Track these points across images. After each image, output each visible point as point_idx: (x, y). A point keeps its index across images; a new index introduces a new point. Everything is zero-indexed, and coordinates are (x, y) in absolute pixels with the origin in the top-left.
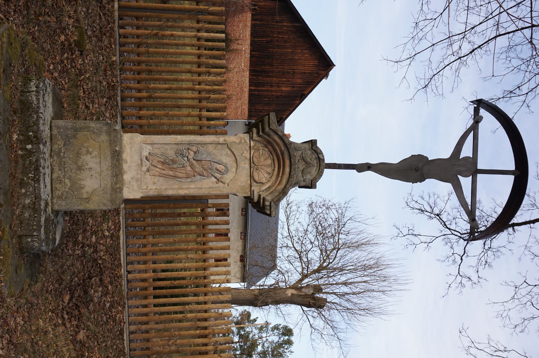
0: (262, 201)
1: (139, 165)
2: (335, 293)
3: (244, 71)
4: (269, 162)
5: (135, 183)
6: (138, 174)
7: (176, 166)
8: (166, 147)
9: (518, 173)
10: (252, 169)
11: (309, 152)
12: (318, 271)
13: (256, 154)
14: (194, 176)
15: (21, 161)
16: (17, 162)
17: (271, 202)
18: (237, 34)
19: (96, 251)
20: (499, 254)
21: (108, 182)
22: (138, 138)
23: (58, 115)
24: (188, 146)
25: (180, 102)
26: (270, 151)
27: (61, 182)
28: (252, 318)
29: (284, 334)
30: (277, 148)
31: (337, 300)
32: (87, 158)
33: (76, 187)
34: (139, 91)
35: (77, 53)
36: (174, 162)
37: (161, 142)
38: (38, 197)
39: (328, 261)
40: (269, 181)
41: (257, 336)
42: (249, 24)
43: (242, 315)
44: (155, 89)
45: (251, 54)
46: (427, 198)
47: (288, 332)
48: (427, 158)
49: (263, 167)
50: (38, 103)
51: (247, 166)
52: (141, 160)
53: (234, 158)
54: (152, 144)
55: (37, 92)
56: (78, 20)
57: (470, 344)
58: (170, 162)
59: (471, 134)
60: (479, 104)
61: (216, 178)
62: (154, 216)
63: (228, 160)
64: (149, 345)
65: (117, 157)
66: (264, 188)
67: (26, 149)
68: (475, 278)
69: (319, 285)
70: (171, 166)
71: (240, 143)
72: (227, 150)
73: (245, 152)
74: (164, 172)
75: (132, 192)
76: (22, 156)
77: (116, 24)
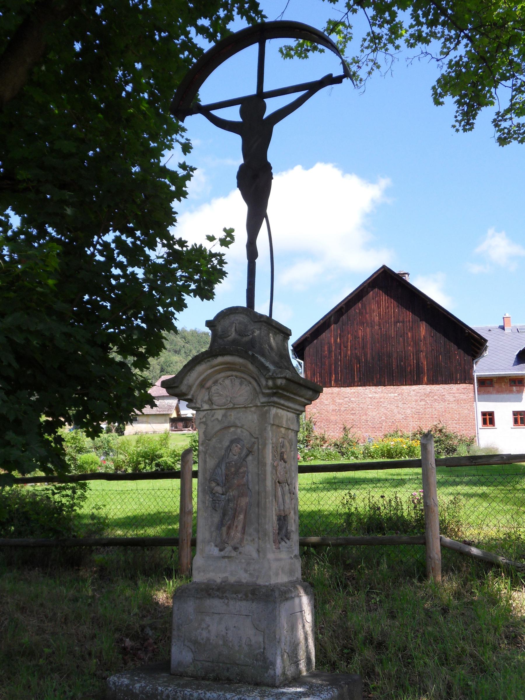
30: (205, 374)
48: (242, 167)
52: (224, 557)
59: (215, 113)
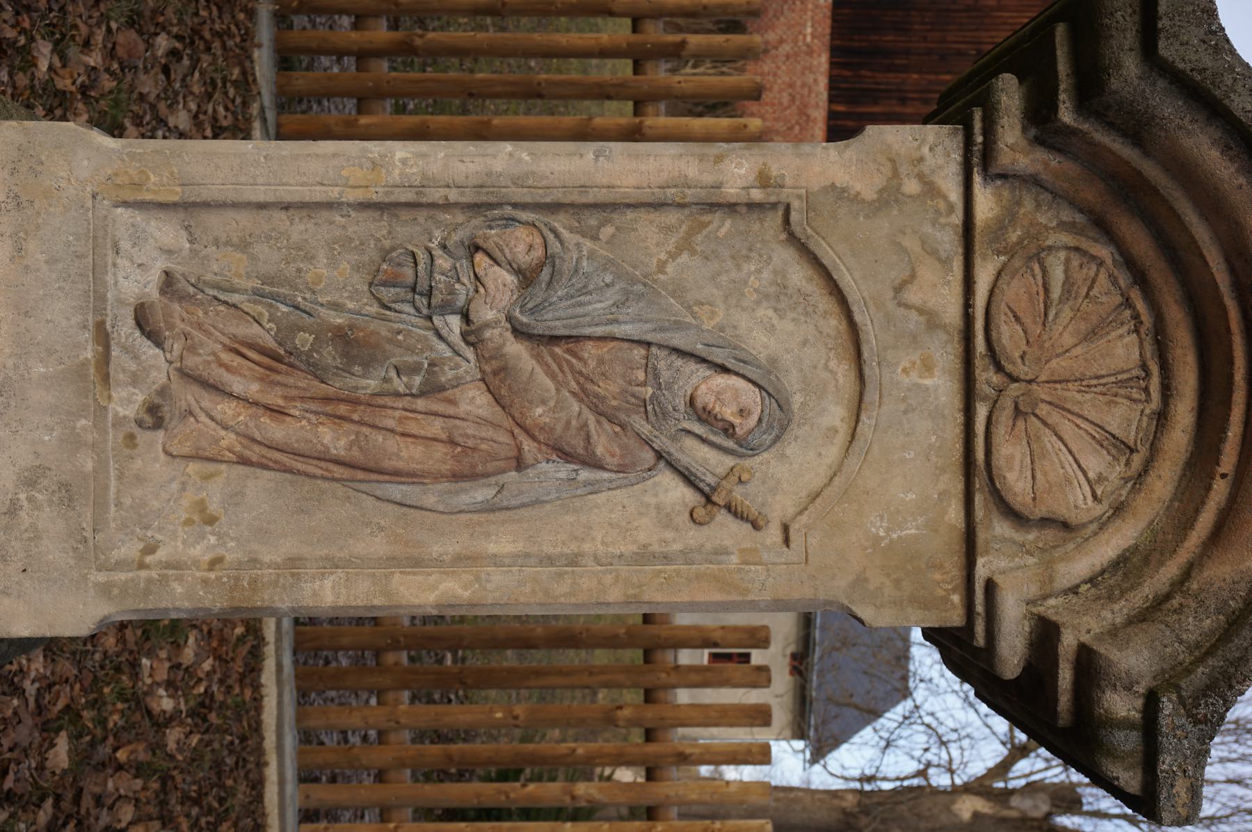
0: (1065, 676)
3: (810, 52)
4: (1123, 350)
6: (73, 442)
7: (372, 384)
8: (299, 229)
10: (982, 412)
13: (1016, 291)
14: (520, 464)
17: (1151, 701)
24: (466, 228)
25: (543, 73)
26: (1130, 263)
30: (1201, 232)
36: (353, 347)
37: (260, 195)
40: (1119, 509)
49: (1072, 394)
51: (943, 386)
52: (103, 336)
53: (834, 323)
54: (187, 208)
58: (329, 355)
61: (688, 478)
63: (786, 334)
70: (338, 385)
71: (889, 197)
72: (784, 256)
73: (928, 272)
74: (276, 431)
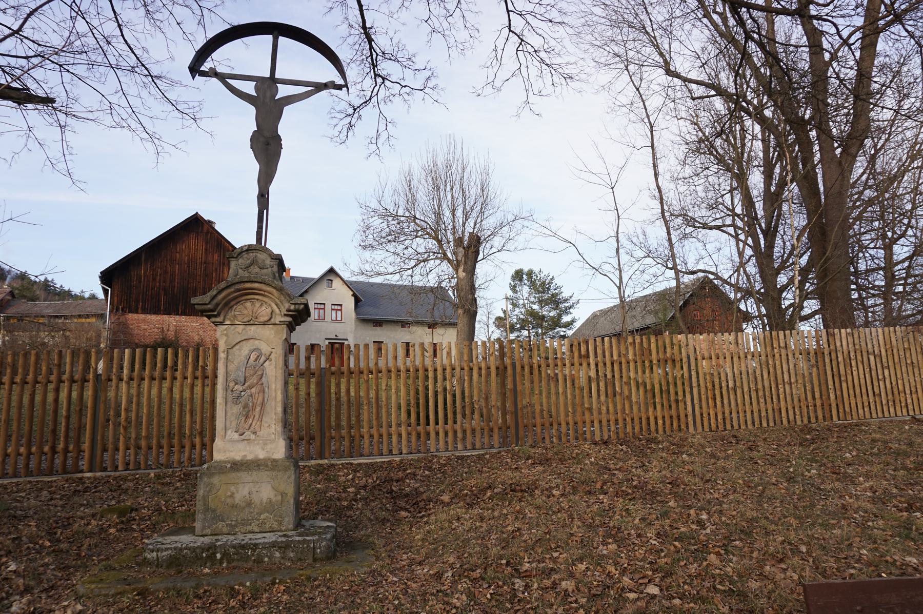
1: (250, 443)
2: (464, 224)
4: (248, 304)
5: (268, 447)
6: (258, 444)
8: (229, 414)
9: (276, 33)
11: (240, 261)
12: (440, 242)
15: (234, 564)
16: (234, 568)
18: (156, 330)
19: (365, 487)
20: (400, 46)
21: (264, 475)
22: (218, 443)
23: (192, 531)
27: (263, 523)
28: (502, 315)
29: (521, 280)
31: (471, 222)
32: (238, 497)
33: (270, 507)
34: (193, 446)
35: (133, 515)
36: (245, 406)
38: (274, 544)
39: (428, 230)
41: (523, 310)
42: (142, 316)
43: (498, 327)
44: (192, 428)
45: (181, 315)
46: (335, 121)
47: (518, 275)
50: (171, 549)
51: (253, 328)
54: (226, 429)
55: (158, 551)
56: (93, 515)
57: (490, 86)
60: (195, 69)
62: (338, 427)
63: (245, 349)
64: (478, 429)
65: (237, 466)
66: (277, 310)
67: (222, 559)
68: (428, 74)
69: (455, 240)
71: (226, 335)
72: (234, 349)
74: (257, 417)
75: (279, 450)
76: (229, 563)
77: (112, 474)
